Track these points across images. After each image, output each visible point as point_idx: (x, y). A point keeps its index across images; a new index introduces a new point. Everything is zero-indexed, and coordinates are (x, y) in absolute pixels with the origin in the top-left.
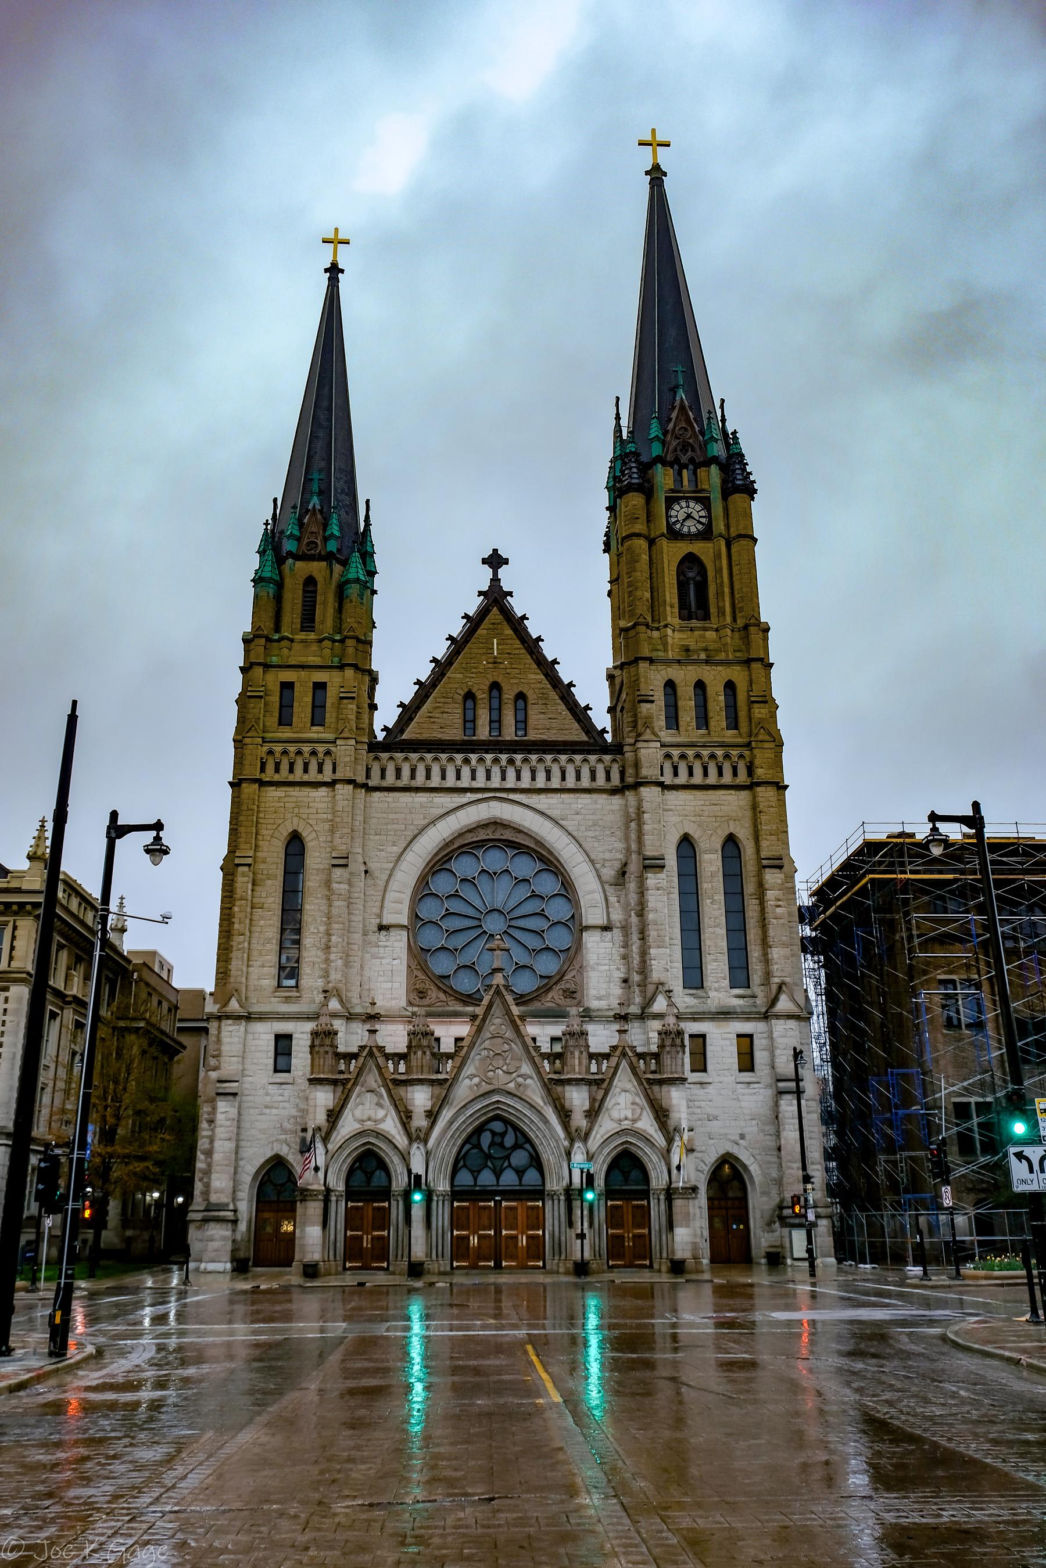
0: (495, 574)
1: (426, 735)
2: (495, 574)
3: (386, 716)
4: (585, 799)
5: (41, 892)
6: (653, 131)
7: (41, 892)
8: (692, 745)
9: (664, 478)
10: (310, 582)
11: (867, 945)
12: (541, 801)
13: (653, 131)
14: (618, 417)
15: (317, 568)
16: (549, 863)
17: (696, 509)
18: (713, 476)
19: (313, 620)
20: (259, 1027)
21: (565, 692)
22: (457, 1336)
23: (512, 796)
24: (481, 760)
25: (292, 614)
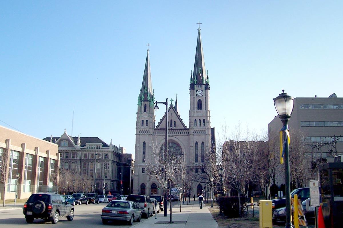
0: (172, 102)
1: (162, 127)
2: (172, 102)
3: (157, 124)
4: (183, 136)
5: (280, 192)
6: (201, 24)
7: (280, 192)
8: (204, 129)
9: (196, 87)
10: (145, 104)
11: (239, 162)
12: (177, 137)
13: (201, 24)
14: (191, 76)
15: (146, 103)
16: (178, 145)
17: (201, 92)
18: (204, 86)
19: (146, 111)
20: (140, 167)
21: (181, 120)
22: (130, 181)
23: (173, 136)
24: (163, 131)
25: (143, 109)
